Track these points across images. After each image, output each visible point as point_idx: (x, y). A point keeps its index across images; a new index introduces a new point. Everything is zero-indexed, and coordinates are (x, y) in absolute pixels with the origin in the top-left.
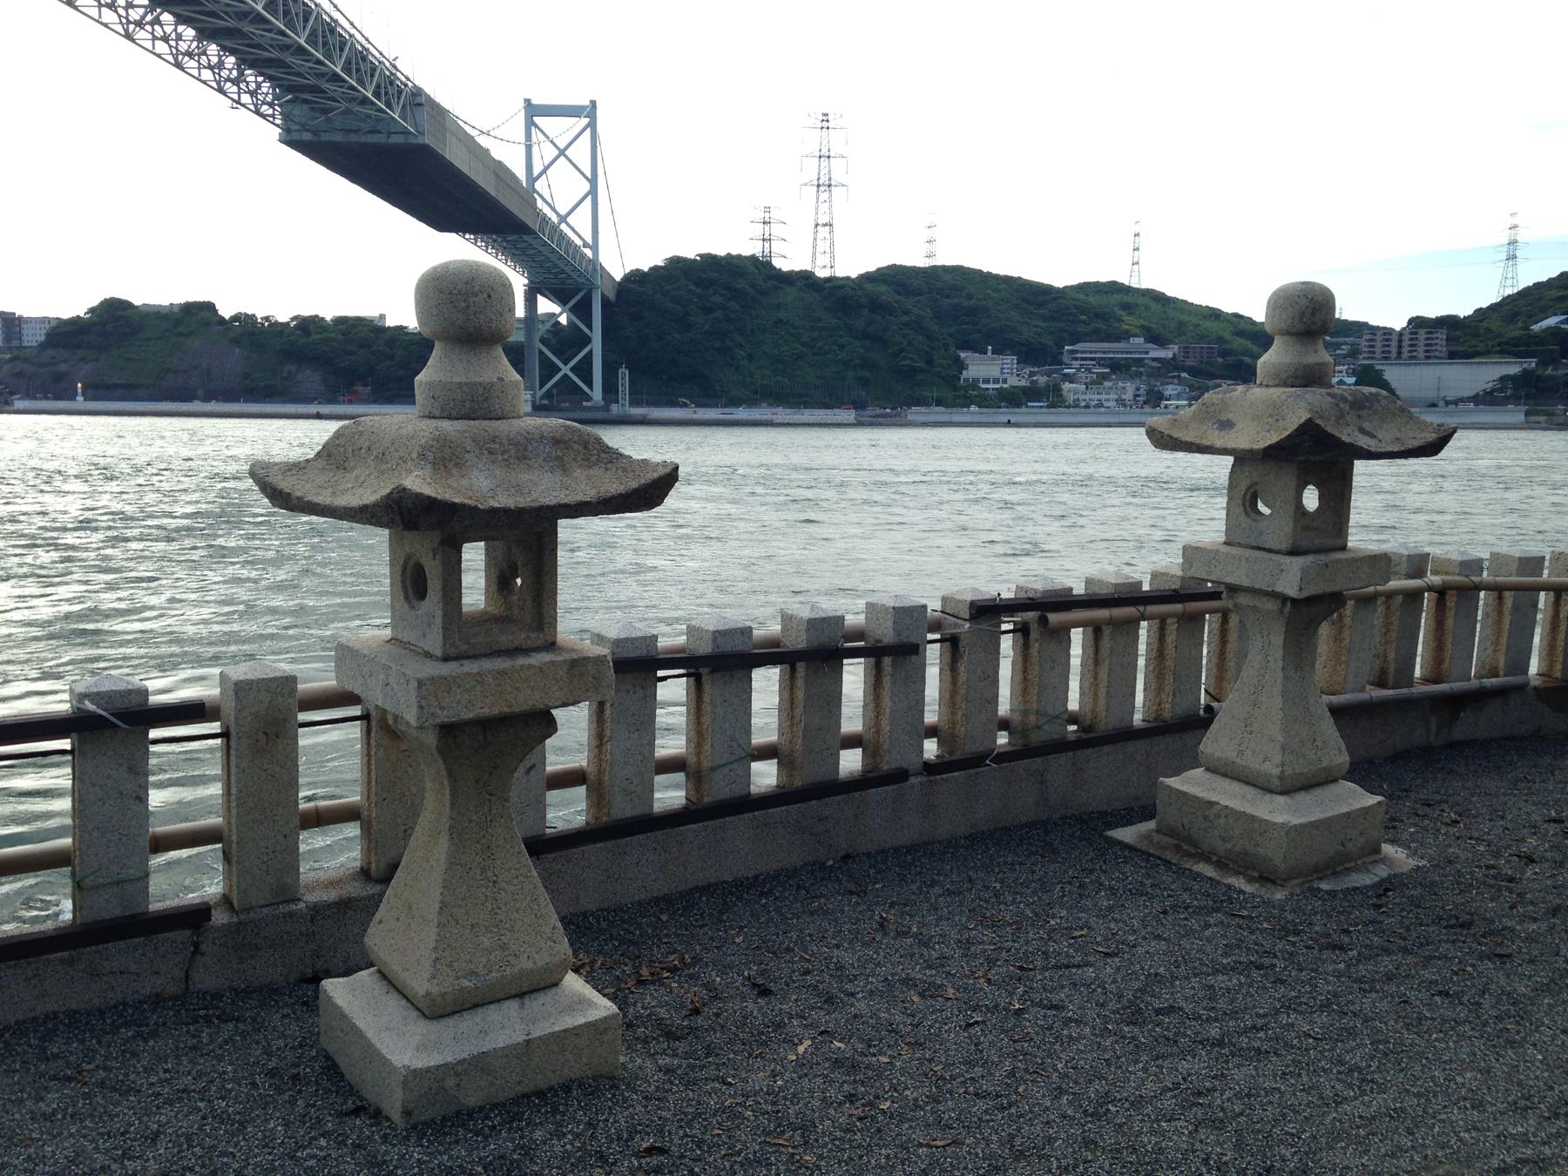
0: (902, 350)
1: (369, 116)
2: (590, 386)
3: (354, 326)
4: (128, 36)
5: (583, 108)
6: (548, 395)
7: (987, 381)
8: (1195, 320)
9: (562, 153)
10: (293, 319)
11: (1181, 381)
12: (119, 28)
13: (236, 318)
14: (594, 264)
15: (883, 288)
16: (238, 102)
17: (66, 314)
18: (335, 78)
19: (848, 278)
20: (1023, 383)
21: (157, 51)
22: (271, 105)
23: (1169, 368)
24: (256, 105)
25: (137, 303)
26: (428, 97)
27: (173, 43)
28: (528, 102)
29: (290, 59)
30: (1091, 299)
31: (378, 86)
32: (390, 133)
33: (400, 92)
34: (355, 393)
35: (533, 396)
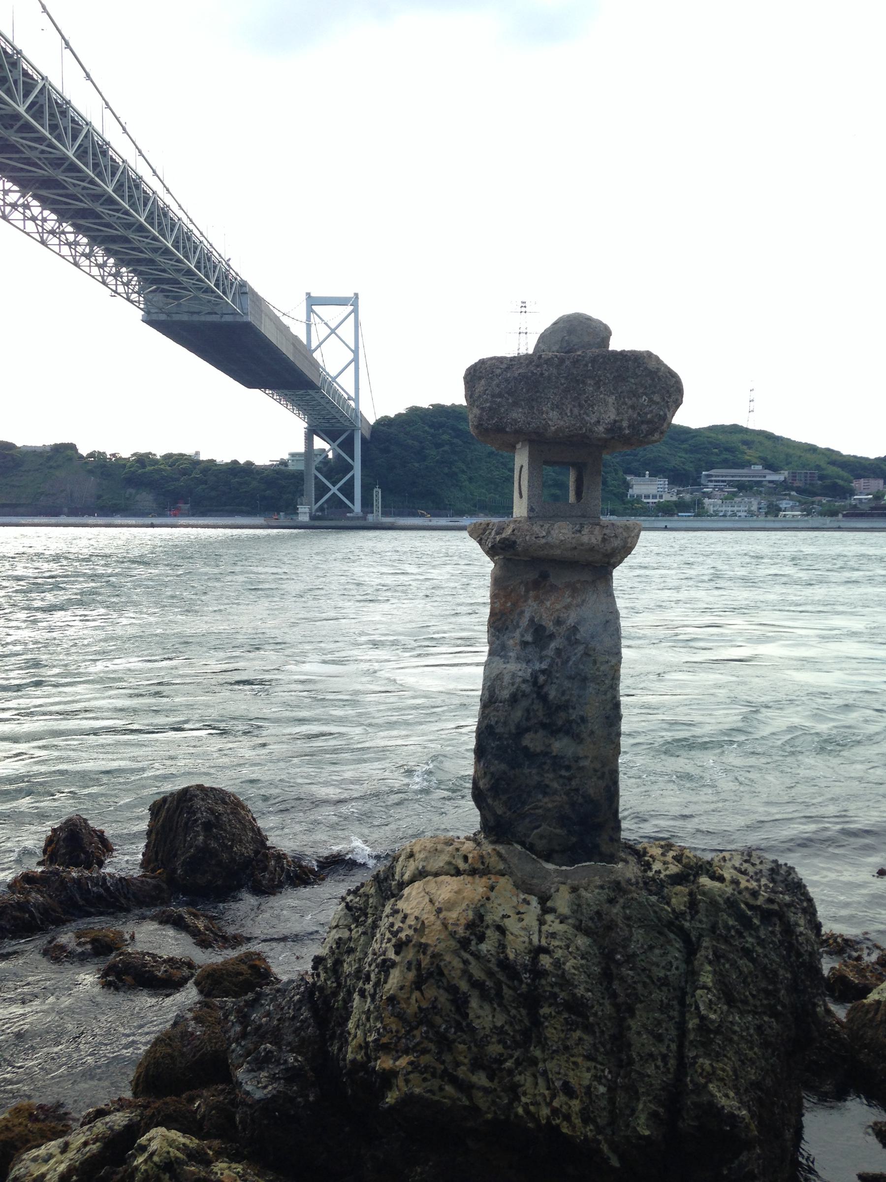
1: (209, 301)
2: (353, 502)
3: (177, 460)
4: (43, 242)
5: (350, 298)
6: (321, 509)
7: (647, 497)
8: (799, 453)
9: (333, 331)
10: (133, 455)
11: (792, 498)
12: (37, 236)
13: (92, 455)
14: (356, 411)
16: (115, 292)
18: (189, 272)
20: (675, 498)
23: (783, 487)
25: (19, 444)
26: (251, 288)
27: (39, 223)
28: (308, 294)
30: (720, 437)
34: (179, 509)
35: (310, 509)
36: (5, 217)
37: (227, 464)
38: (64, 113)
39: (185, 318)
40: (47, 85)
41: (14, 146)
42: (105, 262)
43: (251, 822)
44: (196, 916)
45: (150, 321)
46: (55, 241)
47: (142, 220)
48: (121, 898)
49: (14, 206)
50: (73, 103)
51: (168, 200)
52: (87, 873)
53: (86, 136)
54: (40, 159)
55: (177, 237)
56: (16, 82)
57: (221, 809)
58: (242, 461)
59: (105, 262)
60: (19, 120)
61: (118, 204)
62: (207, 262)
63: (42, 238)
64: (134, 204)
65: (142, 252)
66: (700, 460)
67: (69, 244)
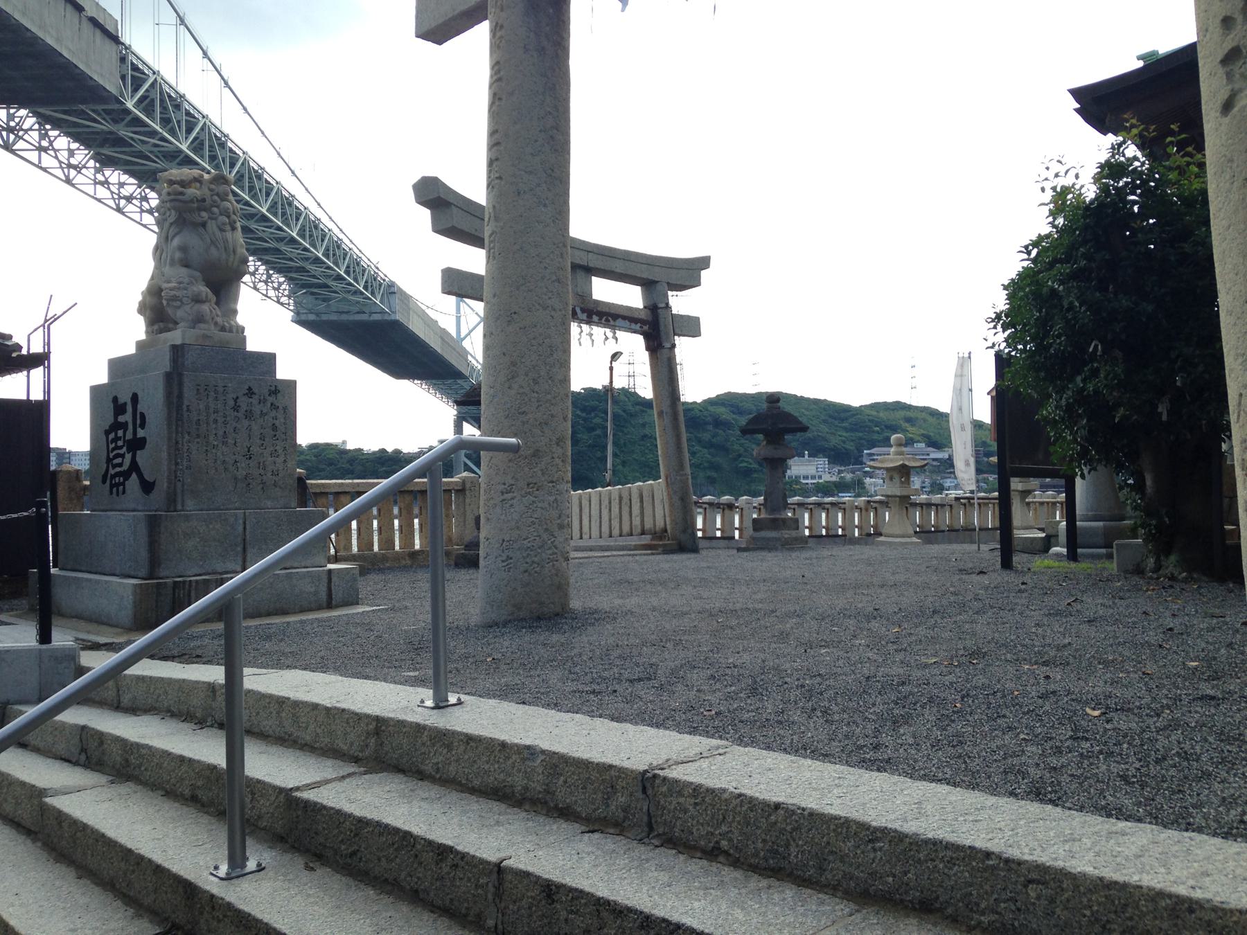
0: (740, 456)
1: (358, 302)
3: (323, 450)
4: (119, 210)
15: (721, 410)
18: (317, 260)
19: (695, 403)
20: (834, 479)
21: (43, 165)
26: (399, 289)
30: (881, 415)
31: (348, 267)
32: (371, 313)
33: (380, 285)
36: (8, 147)
37: (374, 453)
38: (178, 107)
39: (334, 317)
40: (159, 79)
49: (129, 199)
50: (188, 97)
51: (319, 213)
53: (202, 129)
55: (303, 226)
58: (390, 450)
60: (176, 157)
61: (271, 221)
62: (356, 267)
66: (861, 438)
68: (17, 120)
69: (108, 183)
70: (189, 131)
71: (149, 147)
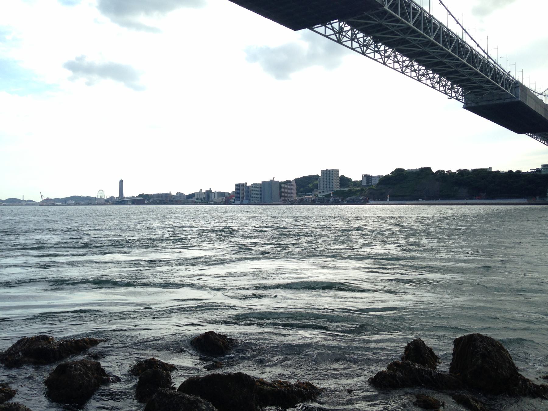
1: (498, 94)
10: (457, 171)
13: (438, 172)
16: (451, 96)
17: (384, 174)
22: (462, 96)
24: (445, 91)
25: (406, 169)
27: (417, 72)
29: (445, 60)
31: (503, 83)
32: (505, 99)
37: (506, 173)
41: (407, 41)
42: (446, 84)
43: (508, 359)
44: (476, 401)
45: (467, 107)
46: (424, 78)
47: (465, 61)
48: (439, 383)
49: (407, 67)
50: (467, 42)
52: (422, 367)
53: (439, 29)
54: (418, 44)
55: (469, 57)
56: (409, 13)
57: (490, 348)
59: (446, 84)
60: (385, 15)
63: (418, 78)
64: (461, 55)
65: (464, 76)
67: (430, 79)
68: (367, 42)
69: (380, 51)
70: (434, 32)
71: (417, 42)
